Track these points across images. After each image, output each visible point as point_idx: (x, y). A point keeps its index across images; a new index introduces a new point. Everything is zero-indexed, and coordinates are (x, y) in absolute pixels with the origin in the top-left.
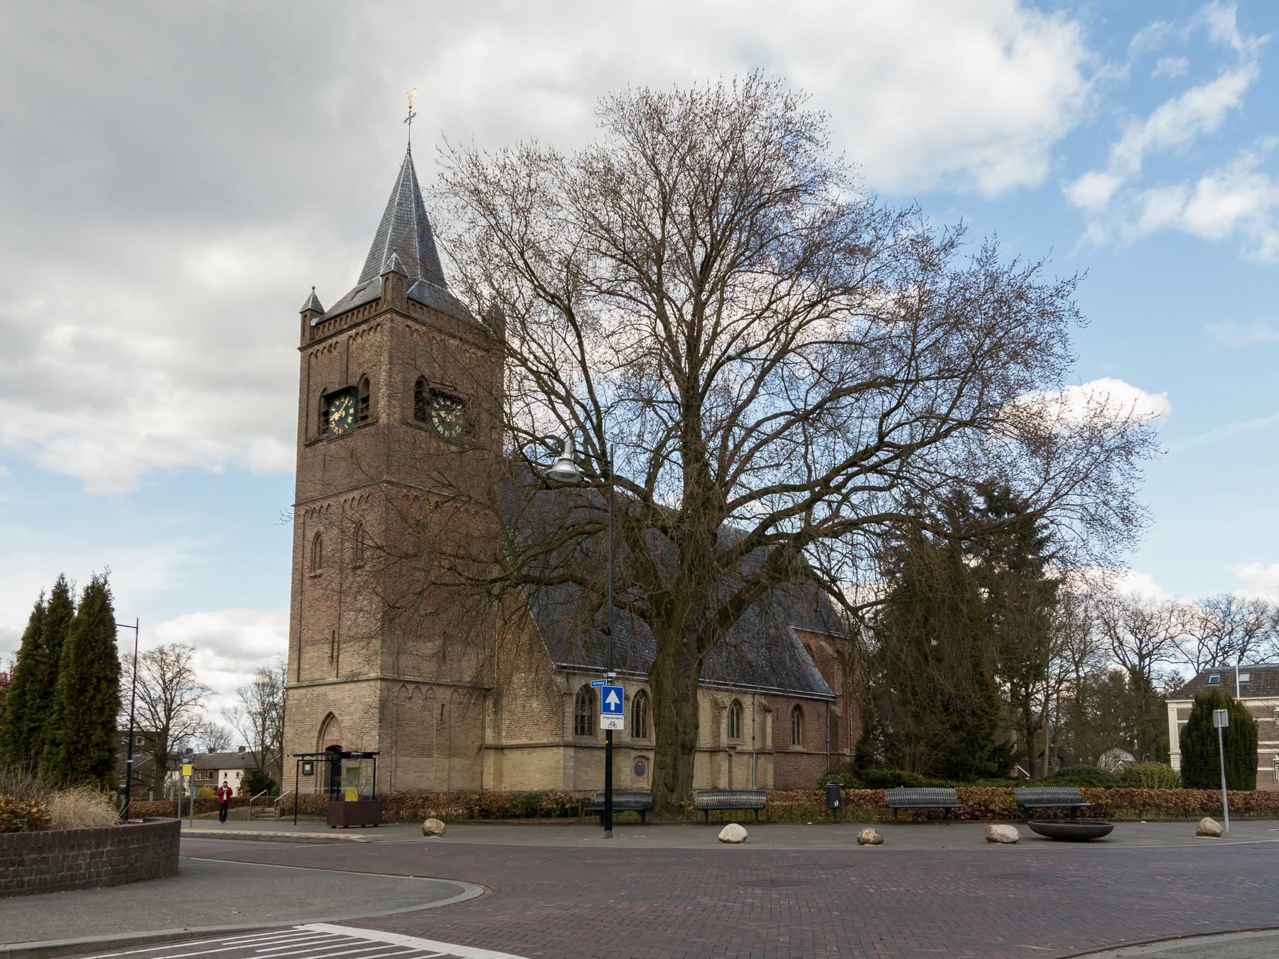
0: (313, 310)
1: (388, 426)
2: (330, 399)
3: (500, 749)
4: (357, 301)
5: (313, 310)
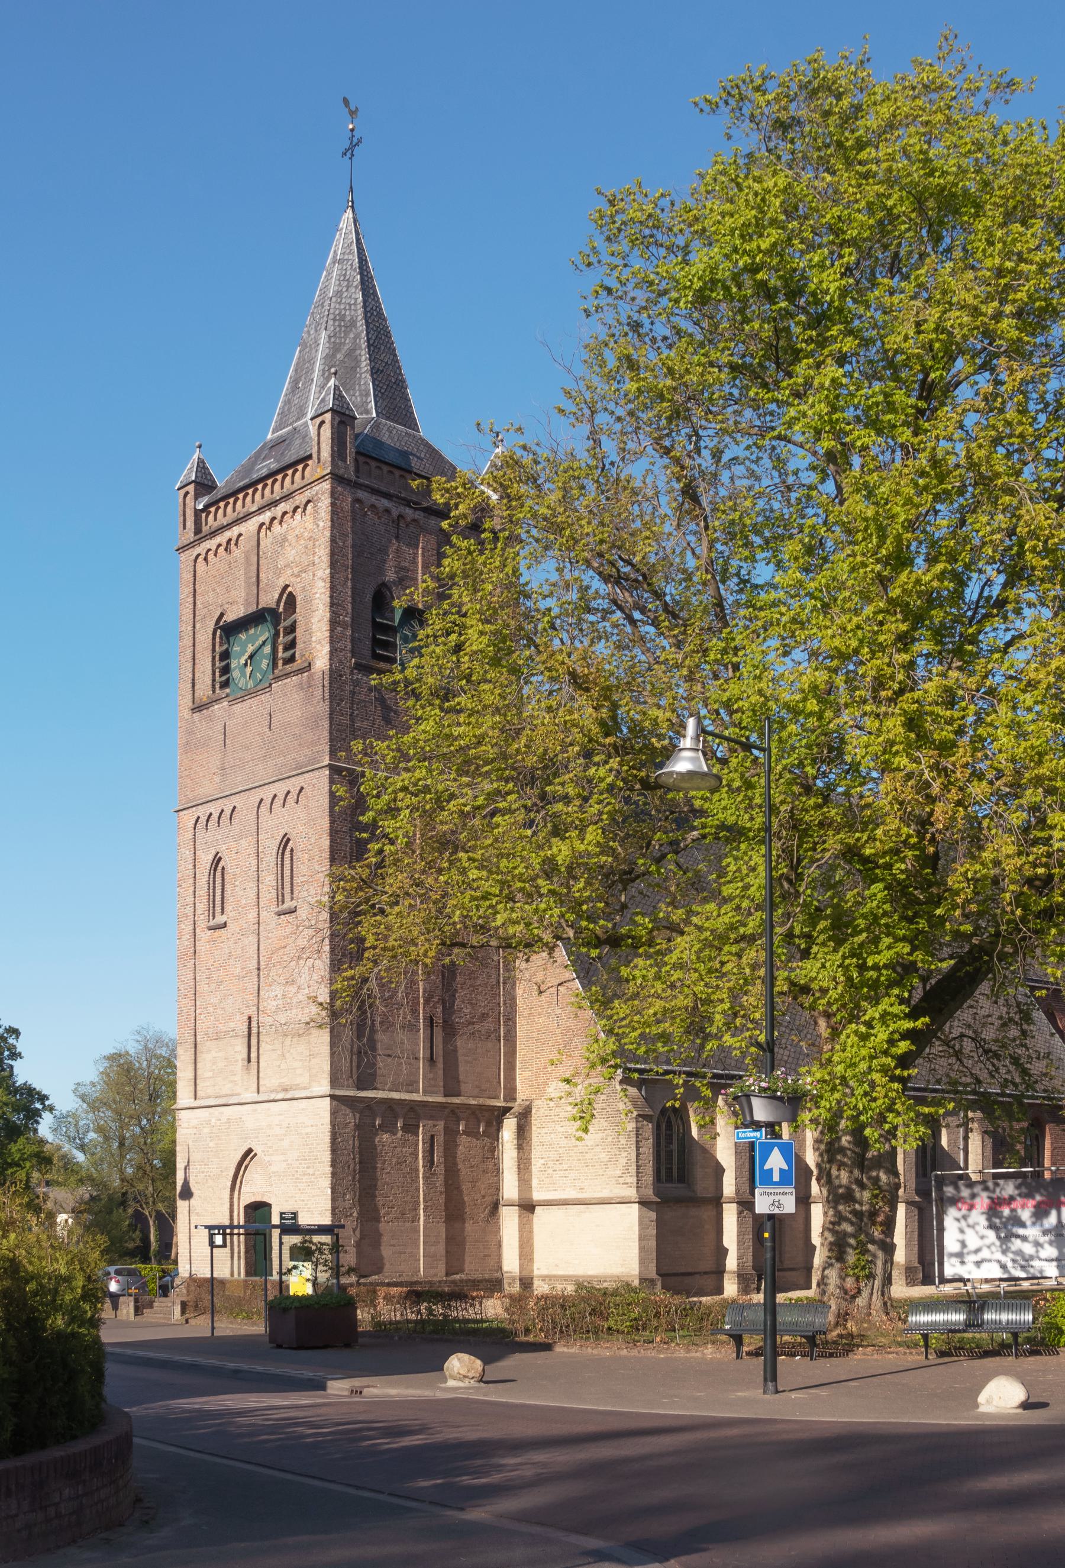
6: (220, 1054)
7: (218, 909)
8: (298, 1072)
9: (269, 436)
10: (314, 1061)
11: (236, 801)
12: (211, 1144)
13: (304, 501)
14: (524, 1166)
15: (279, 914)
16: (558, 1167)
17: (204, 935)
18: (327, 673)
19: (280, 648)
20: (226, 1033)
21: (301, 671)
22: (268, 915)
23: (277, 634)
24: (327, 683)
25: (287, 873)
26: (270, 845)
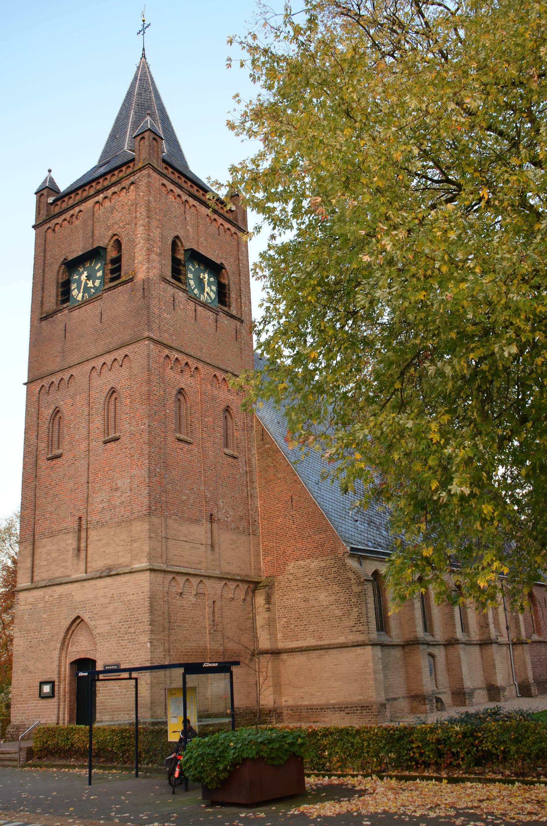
0: (48, 190)
1: (146, 281)
2: (72, 265)
3: (276, 653)
4: (102, 170)
5: (48, 190)
6: (55, 547)
8: (121, 554)
10: (135, 545)
11: (73, 371)
12: (45, 616)
14: (271, 623)
15: (105, 442)
20: (60, 531)
21: (126, 282)
22: (97, 444)
25: (112, 414)
26: (99, 397)
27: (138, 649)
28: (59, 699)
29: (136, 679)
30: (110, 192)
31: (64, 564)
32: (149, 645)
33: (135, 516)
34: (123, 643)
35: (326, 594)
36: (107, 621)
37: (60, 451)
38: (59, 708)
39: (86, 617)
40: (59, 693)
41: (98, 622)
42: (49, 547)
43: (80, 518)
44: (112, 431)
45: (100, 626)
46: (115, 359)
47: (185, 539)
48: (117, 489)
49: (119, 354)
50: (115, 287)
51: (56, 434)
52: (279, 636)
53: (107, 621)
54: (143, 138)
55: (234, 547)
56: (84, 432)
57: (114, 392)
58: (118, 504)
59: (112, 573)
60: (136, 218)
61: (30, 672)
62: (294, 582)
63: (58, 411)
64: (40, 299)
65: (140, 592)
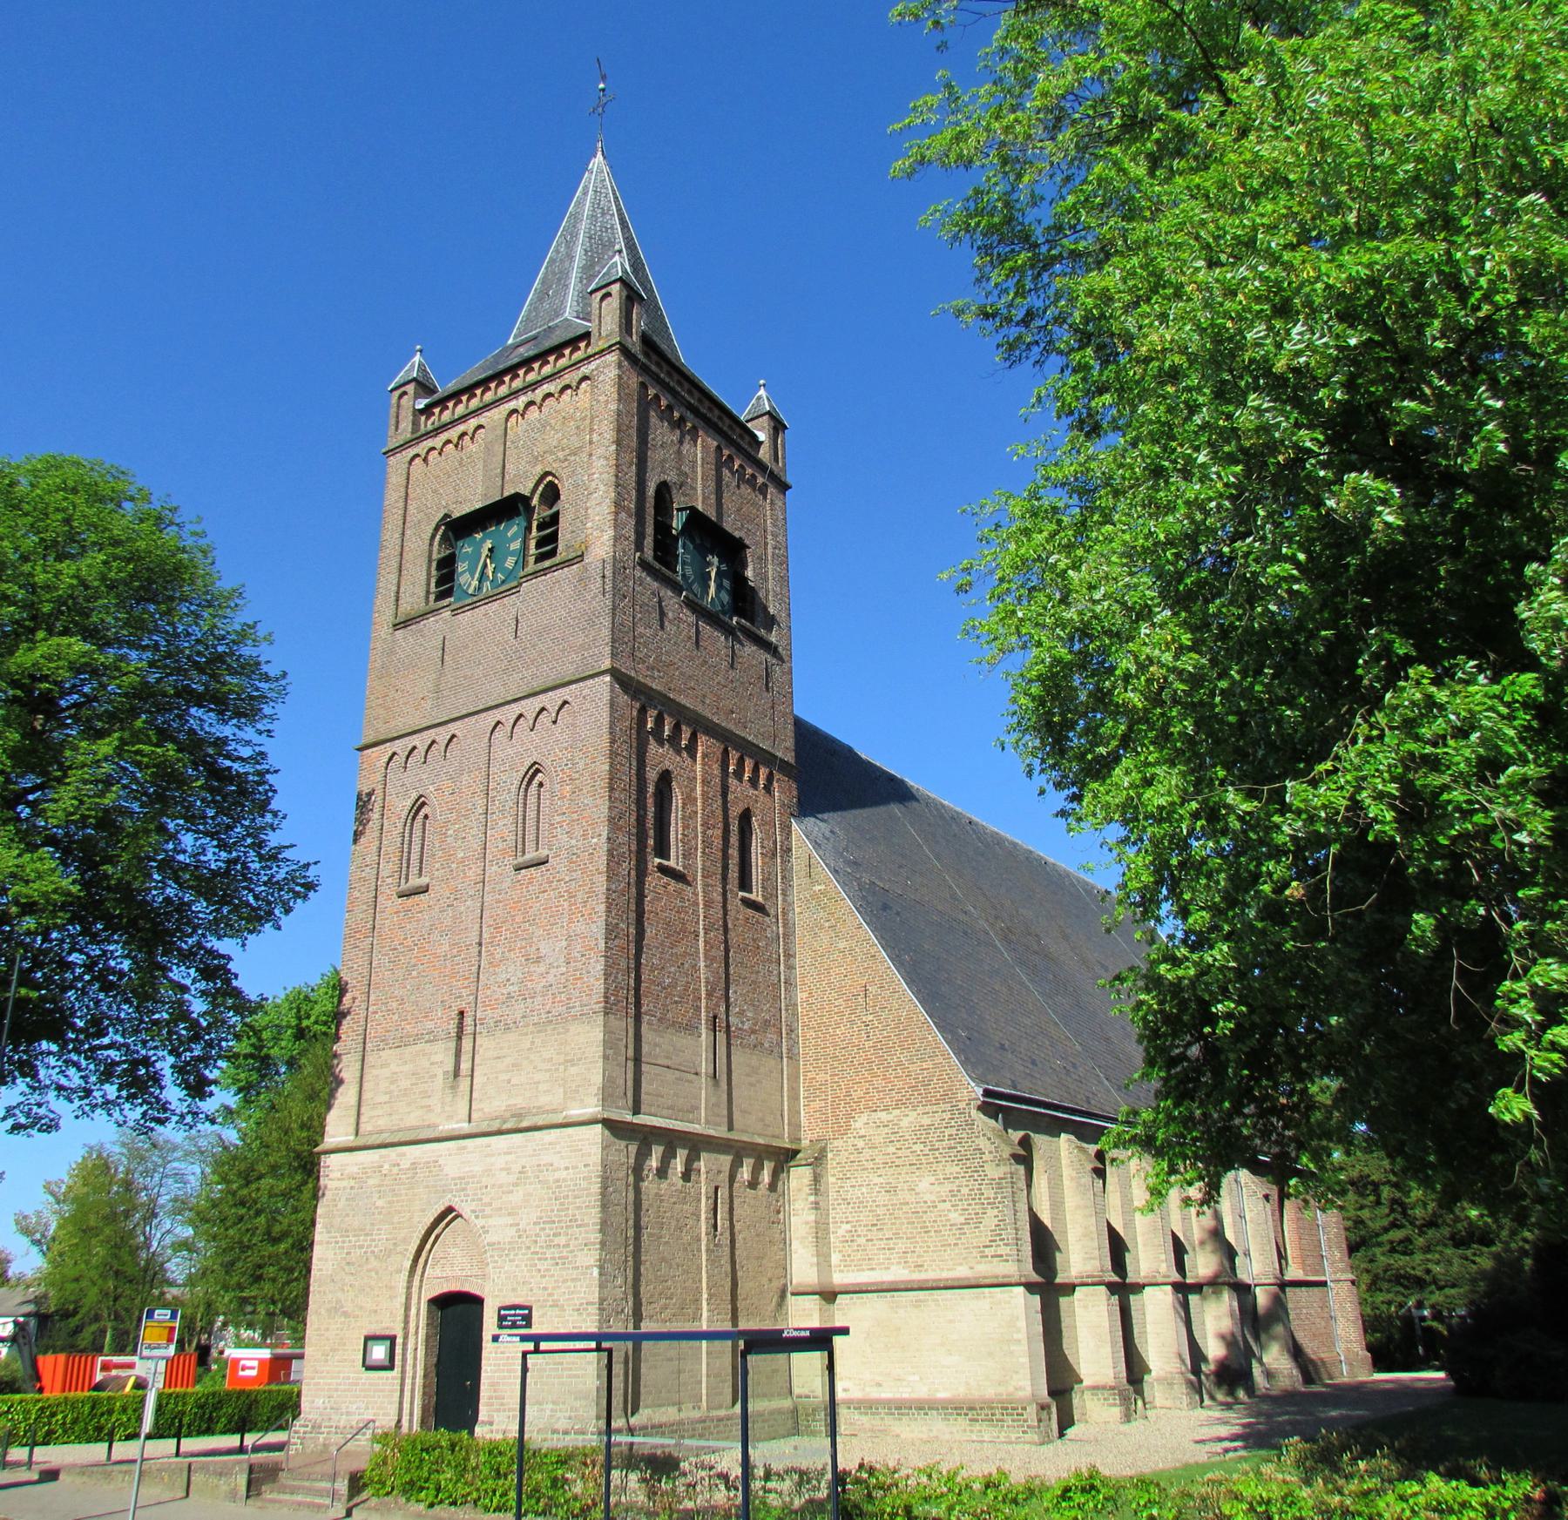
6: (406, 1068)
7: (414, 870)
8: (543, 1087)
9: (510, 341)
10: (573, 1070)
13: (577, 379)
14: (821, 1233)
15: (518, 869)
16: (874, 1234)
17: (389, 902)
18: (609, 560)
19: (533, 543)
23: (528, 529)
24: (608, 573)
25: (531, 814)
27: (573, 1280)
28: (403, 1372)
29: (610, 1351)
30: (539, 394)
31: (426, 1102)
32: (596, 1272)
33: (576, 1011)
34: (542, 1266)
35: (932, 1179)
36: (510, 1220)
37: (424, 880)
38: (402, 1391)
39: (464, 1208)
40: (404, 1360)
41: (491, 1221)
42: (393, 1067)
43: (462, 1013)
44: (530, 845)
45: (498, 1229)
46: (543, 709)
47: (666, 1062)
48: (538, 960)
49: (551, 700)
50: (545, 571)
51: (416, 848)
52: (835, 1258)
53: (510, 1220)
54: (608, 295)
55: (753, 1080)
56: (476, 845)
57: (538, 771)
58: (539, 988)
59: (525, 1124)
60: (591, 442)
61: (345, 1314)
62: (867, 1153)
63: (424, 804)
64: (394, 588)
65: (581, 1165)
